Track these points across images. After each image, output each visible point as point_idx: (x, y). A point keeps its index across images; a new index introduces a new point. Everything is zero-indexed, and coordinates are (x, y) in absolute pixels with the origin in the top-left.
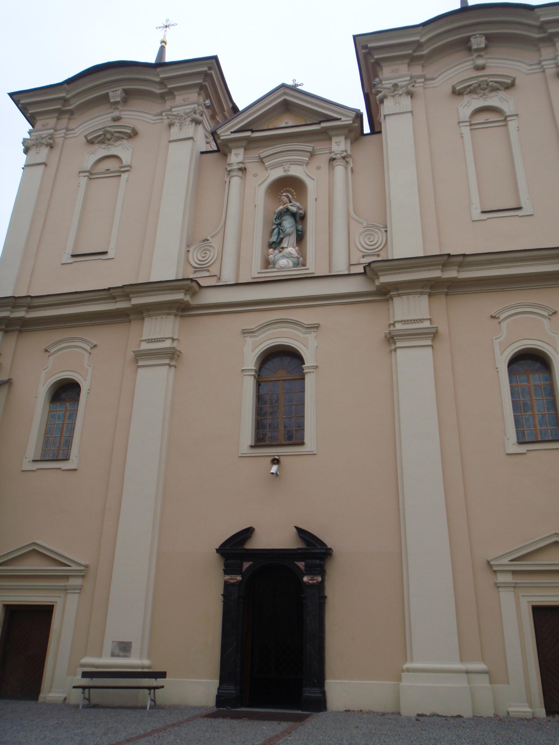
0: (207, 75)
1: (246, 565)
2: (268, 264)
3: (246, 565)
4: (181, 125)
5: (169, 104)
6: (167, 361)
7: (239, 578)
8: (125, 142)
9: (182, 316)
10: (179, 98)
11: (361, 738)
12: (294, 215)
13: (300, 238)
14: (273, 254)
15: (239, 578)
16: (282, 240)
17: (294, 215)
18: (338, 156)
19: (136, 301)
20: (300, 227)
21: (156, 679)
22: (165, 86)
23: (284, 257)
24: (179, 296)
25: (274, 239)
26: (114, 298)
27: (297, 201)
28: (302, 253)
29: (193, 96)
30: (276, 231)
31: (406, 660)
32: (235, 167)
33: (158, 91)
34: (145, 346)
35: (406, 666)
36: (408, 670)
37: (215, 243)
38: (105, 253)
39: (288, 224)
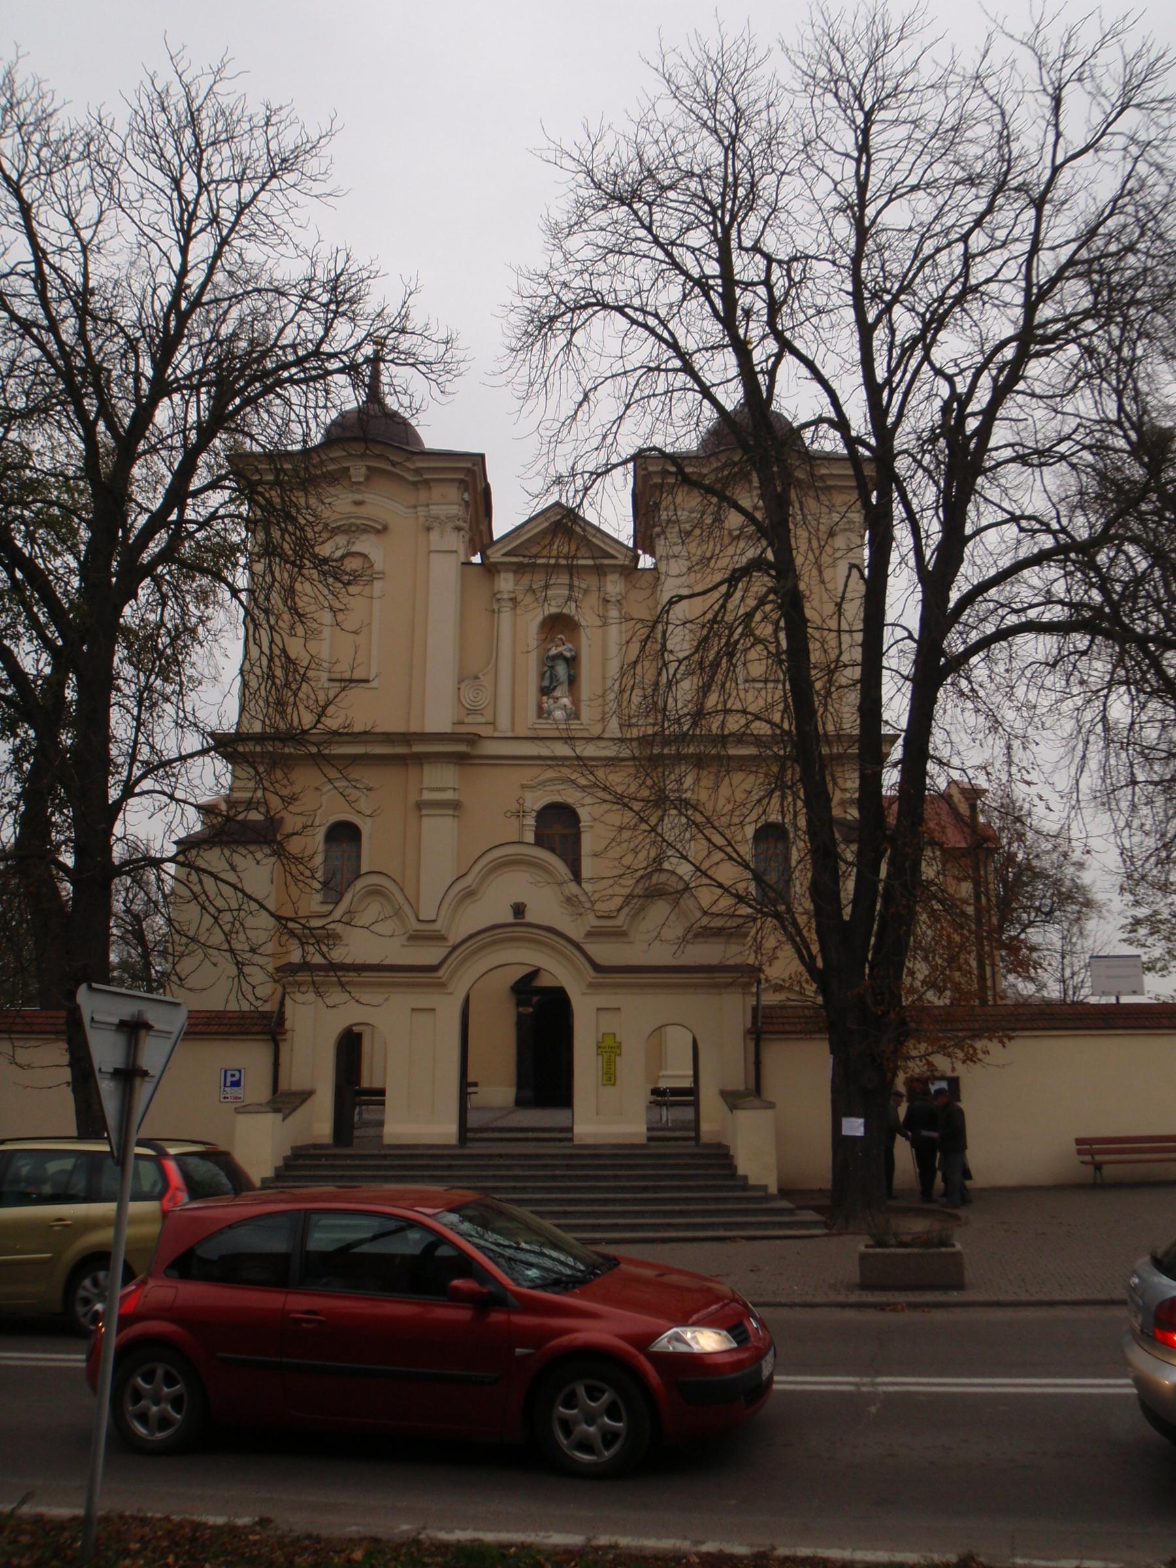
0: (469, 471)
1: (535, 999)
2: (541, 712)
3: (535, 999)
4: (442, 534)
5: (423, 495)
6: (450, 812)
7: (531, 1010)
8: (372, 537)
9: (460, 765)
10: (437, 492)
11: (778, 144)
12: (566, 660)
13: (573, 681)
14: (548, 703)
15: (531, 1010)
16: (555, 688)
17: (566, 660)
18: (613, 599)
19: (418, 748)
20: (572, 672)
21: (861, 645)
22: (421, 475)
23: (559, 708)
24: (462, 748)
25: (546, 683)
26: (393, 742)
27: (570, 642)
28: (576, 702)
29: (453, 493)
30: (548, 674)
31: (661, 1069)
32: (506, 596)
33: (411, 478)
34: (427, 796)
35: (661, 1073)
36: (663, 1076)
37: (486, 680)
38: (367, 681)
39: (561, 670)
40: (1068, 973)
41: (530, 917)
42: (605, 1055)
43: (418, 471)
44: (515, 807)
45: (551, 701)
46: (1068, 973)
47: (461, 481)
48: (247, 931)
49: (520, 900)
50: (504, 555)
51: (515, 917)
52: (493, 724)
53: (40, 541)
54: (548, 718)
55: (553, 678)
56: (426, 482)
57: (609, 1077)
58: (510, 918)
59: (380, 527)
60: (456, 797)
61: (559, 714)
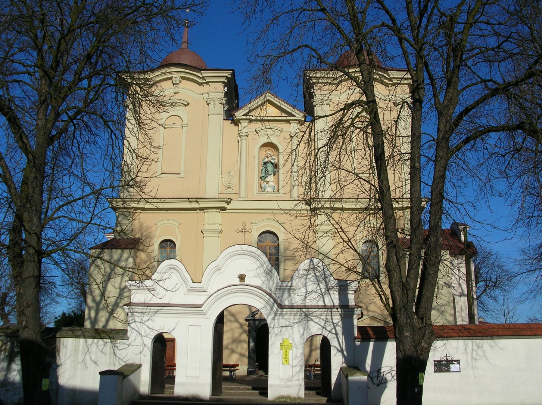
6: (217, 235)
14: (264, 184)
24: (223, 205)
25: (263, 175)
34: (206, 227)
39: (270, 168)
40: (506, 312)
41: (247, 281)
42: (284, 350)
43: (203, 78)
44: (240, 227)
45: (265, 183)
46: (506, 312)
47: (223, 82)
48: (145, 323)
49: (242, 273)
50: (243, 115)
51: (240, 281)
52: (239, 194)
53: (451, 46)
54: (264, 191)
55: (267, 171)
56: (207, 83)
57: (286, 360)
58: (237, 281)
59: (186, 104)
60: (220, 228)
61: (269, 189)
